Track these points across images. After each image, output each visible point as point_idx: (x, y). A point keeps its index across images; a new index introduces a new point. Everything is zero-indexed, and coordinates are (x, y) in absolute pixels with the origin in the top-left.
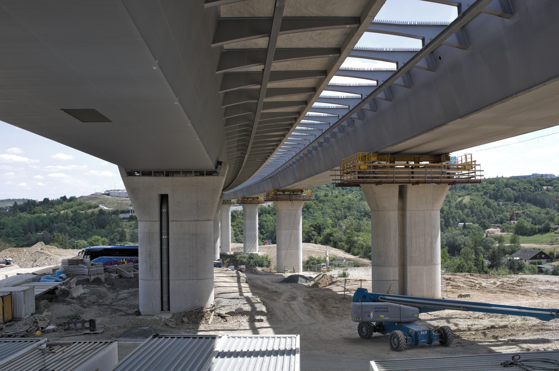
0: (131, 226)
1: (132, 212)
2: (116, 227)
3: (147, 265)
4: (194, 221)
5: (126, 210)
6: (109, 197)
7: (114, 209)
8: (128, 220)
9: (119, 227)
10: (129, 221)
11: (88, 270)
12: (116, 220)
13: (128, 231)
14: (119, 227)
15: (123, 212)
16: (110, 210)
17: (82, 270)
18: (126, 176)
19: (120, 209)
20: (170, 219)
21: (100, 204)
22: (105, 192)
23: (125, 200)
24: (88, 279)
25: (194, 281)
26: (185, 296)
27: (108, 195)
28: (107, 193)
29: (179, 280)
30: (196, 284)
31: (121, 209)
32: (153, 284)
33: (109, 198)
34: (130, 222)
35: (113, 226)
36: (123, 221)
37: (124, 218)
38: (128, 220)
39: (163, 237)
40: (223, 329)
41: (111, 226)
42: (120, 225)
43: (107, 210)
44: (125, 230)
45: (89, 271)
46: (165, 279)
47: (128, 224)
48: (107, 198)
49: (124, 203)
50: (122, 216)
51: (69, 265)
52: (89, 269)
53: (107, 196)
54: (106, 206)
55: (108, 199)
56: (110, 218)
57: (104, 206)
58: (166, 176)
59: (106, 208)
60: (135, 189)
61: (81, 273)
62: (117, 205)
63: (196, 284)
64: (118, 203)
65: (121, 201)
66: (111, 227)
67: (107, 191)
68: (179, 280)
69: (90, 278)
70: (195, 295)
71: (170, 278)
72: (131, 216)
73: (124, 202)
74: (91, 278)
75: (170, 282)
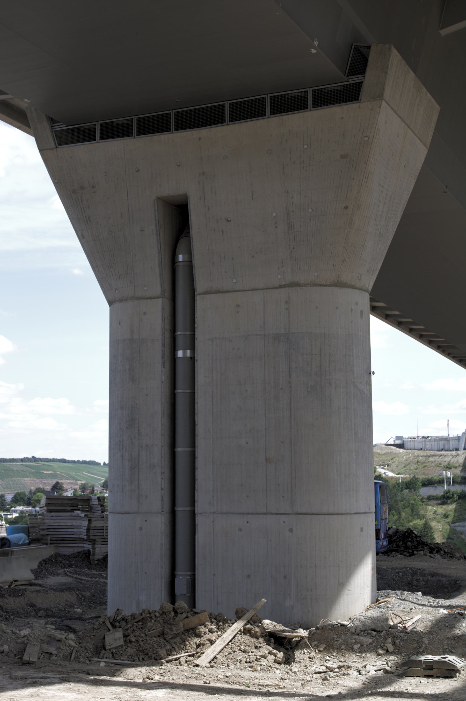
0: (446, 516)
1: (449, 484)
2: (411, 518)
3: (122, 456)
4: (281, 287)
5: (436, 478)
6: (401, 450)
7: (408, 476)
8: (439, 502)
9: (420, 517)
10: (443, 504)
11: (85, 523)
12: (412, 502)
13: (440, 526)
14: (420, 517)
15: (428, 483)
16: (399, 478)
17: (72, 527)
18: (53, 145)
19: (421, 477)
20: (200, 287)
21: (380, 466)
22: (394, 441)
23: (434, 455)
24: (89, 551)
25: (283, 518)
26: (249, 576)
27: (401, 446)
28: (398, 442)
29: (227, 513)
30: (291, 530)
31: (424, 477)
32: (141, 528)
33: (400, 453)
34: (444, 507)
35: (403, 514)
36: (428, 505)
37: (430, 498)
38: (439, 502)
39: (180, 354)
40: (201, 683)
41: (400, 514)
42: (422, 512)
43: (392, 478)
44: (433, 524)
45: (88, 529)
46: (181, 509)
47: (441, 510)
48: (395, 454)
49: (432, 462)
50: (425, 492)
51: (50, 511)
52: (90, 521)
53: (398, 449)
54: (393, 471)
55: (397, 455)
56: (399, 498)
57: (388, 469)
58: (176, 129)
59: (390, 474)
60: (82, 188)
61: (73, 533)
62: (415, 466)
63: (291, 530)
64: (418, 462)
65: (424, 458)
66: (400, 517)
67: (398, 438)
68: (227, 513)
69: (94, 548)
70: (285, 577)
71: (199, 508)
72: (448, 492)
73: (431, 459)
74: (97, 550)
75: (199, 520)
